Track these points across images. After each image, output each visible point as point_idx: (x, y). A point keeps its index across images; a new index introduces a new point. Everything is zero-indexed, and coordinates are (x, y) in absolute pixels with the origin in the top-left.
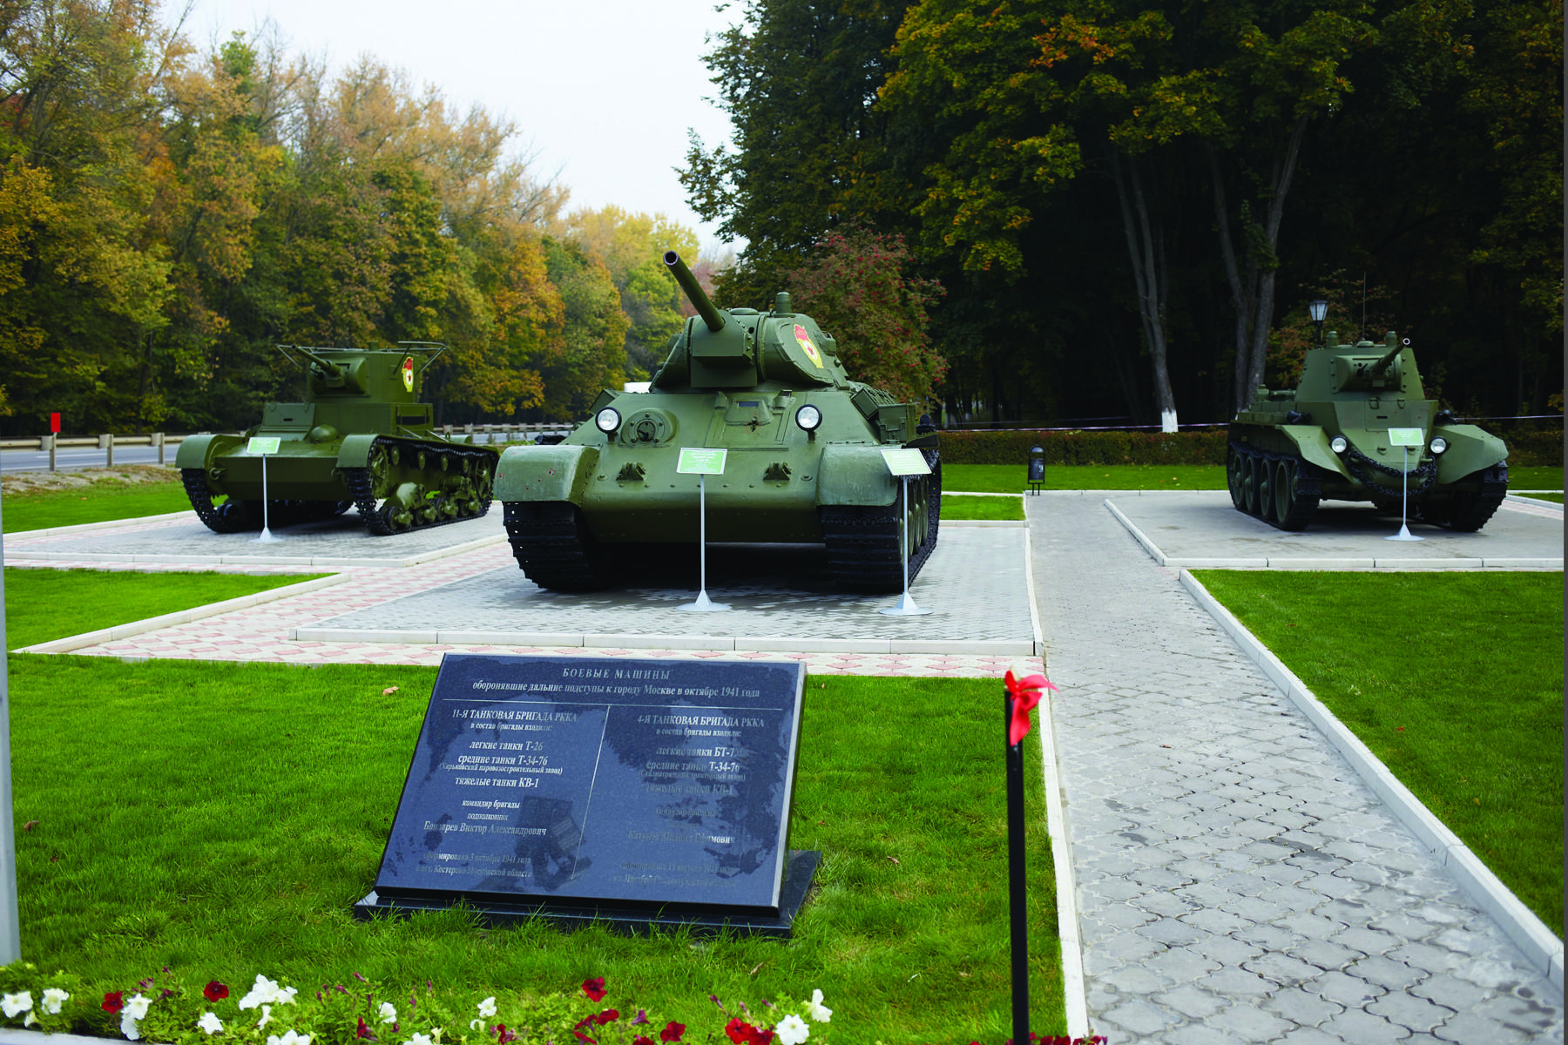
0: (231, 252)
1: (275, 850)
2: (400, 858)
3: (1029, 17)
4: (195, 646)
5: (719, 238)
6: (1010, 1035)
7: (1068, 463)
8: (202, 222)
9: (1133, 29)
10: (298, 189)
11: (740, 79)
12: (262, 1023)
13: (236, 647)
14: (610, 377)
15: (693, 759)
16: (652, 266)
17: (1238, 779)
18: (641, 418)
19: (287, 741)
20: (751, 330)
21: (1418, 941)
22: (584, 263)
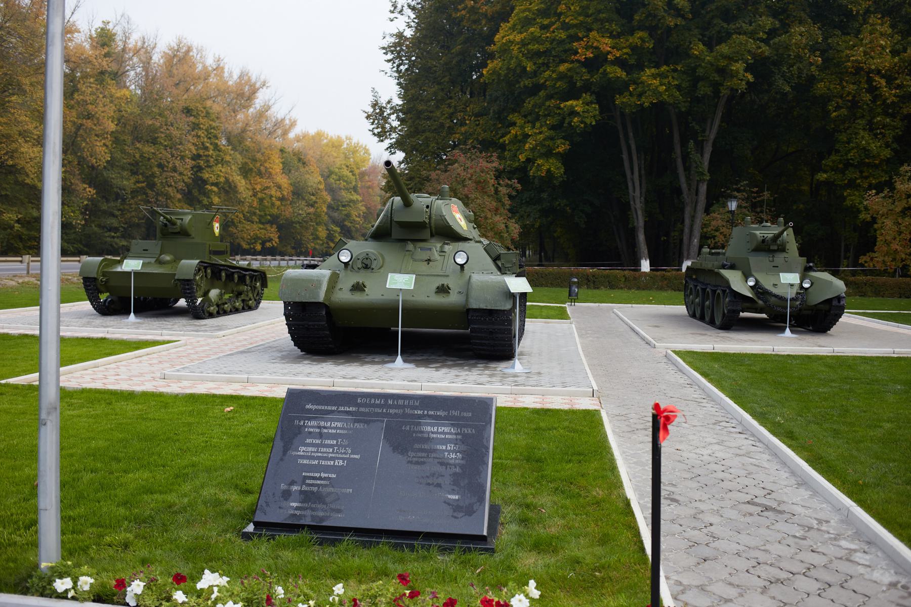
0: (98, 150)
1: (186, 500)
2: (268, 505)
3: (572, 31)
4: (105, 381)
5: (387, 152)
6: (649, 603)
7: (588, 287)
8: (81, 132)
9: (631, 41)
10: (139, 115)
11: (402, 60)
12: (213, 596)
13: (130, 382)
14: (317, 230)
15: (435, 451)
16: (344, 167)
17: (723, 468)
18: (364, 255)
19: (175, 438)
20: (427, 207)
21: (841, 558)
22: (304, 163)
